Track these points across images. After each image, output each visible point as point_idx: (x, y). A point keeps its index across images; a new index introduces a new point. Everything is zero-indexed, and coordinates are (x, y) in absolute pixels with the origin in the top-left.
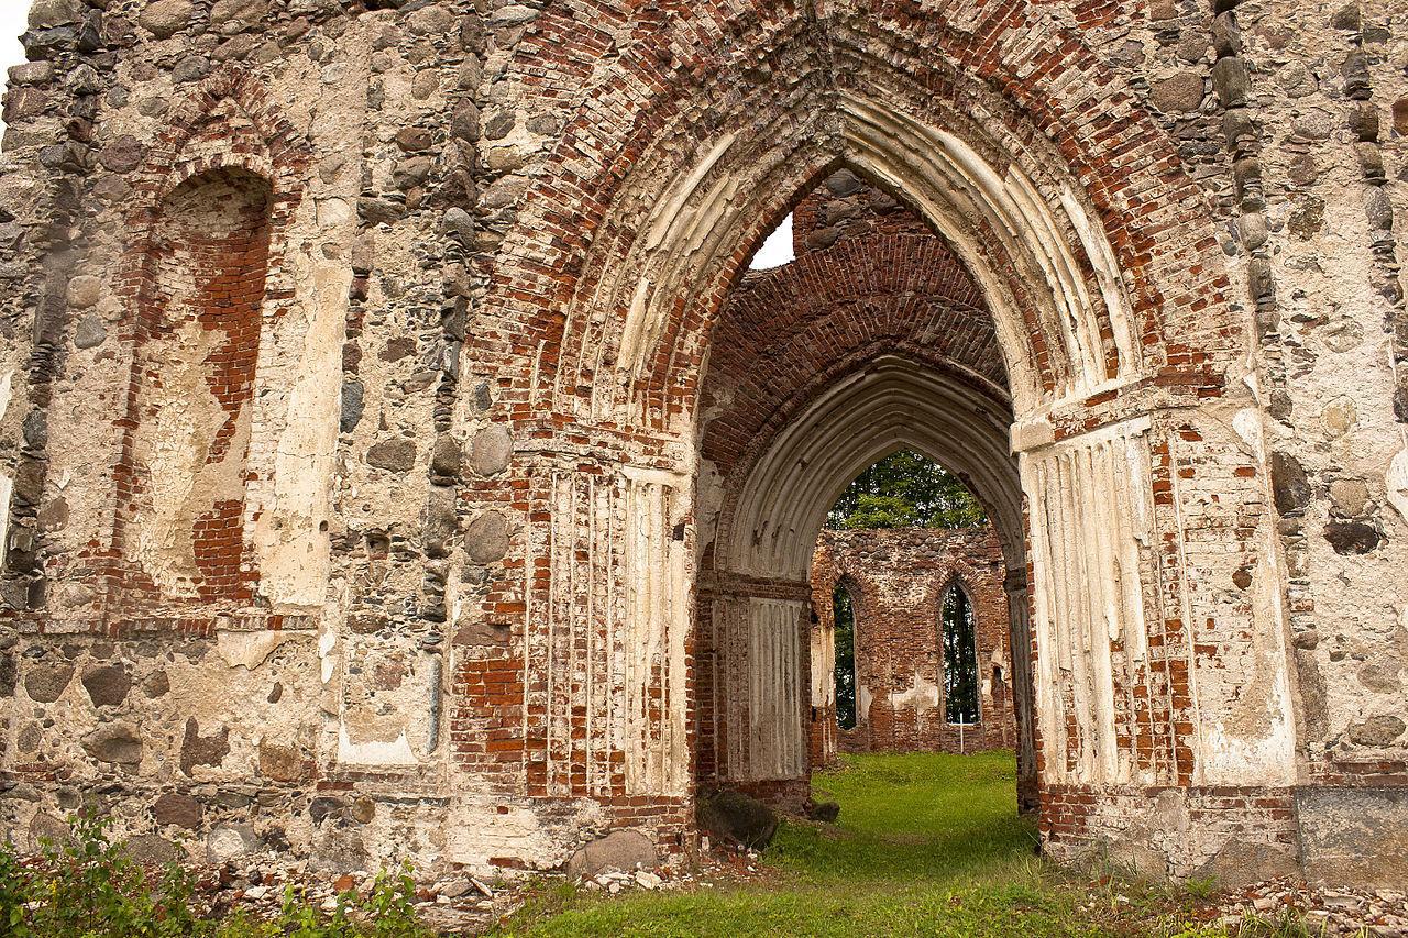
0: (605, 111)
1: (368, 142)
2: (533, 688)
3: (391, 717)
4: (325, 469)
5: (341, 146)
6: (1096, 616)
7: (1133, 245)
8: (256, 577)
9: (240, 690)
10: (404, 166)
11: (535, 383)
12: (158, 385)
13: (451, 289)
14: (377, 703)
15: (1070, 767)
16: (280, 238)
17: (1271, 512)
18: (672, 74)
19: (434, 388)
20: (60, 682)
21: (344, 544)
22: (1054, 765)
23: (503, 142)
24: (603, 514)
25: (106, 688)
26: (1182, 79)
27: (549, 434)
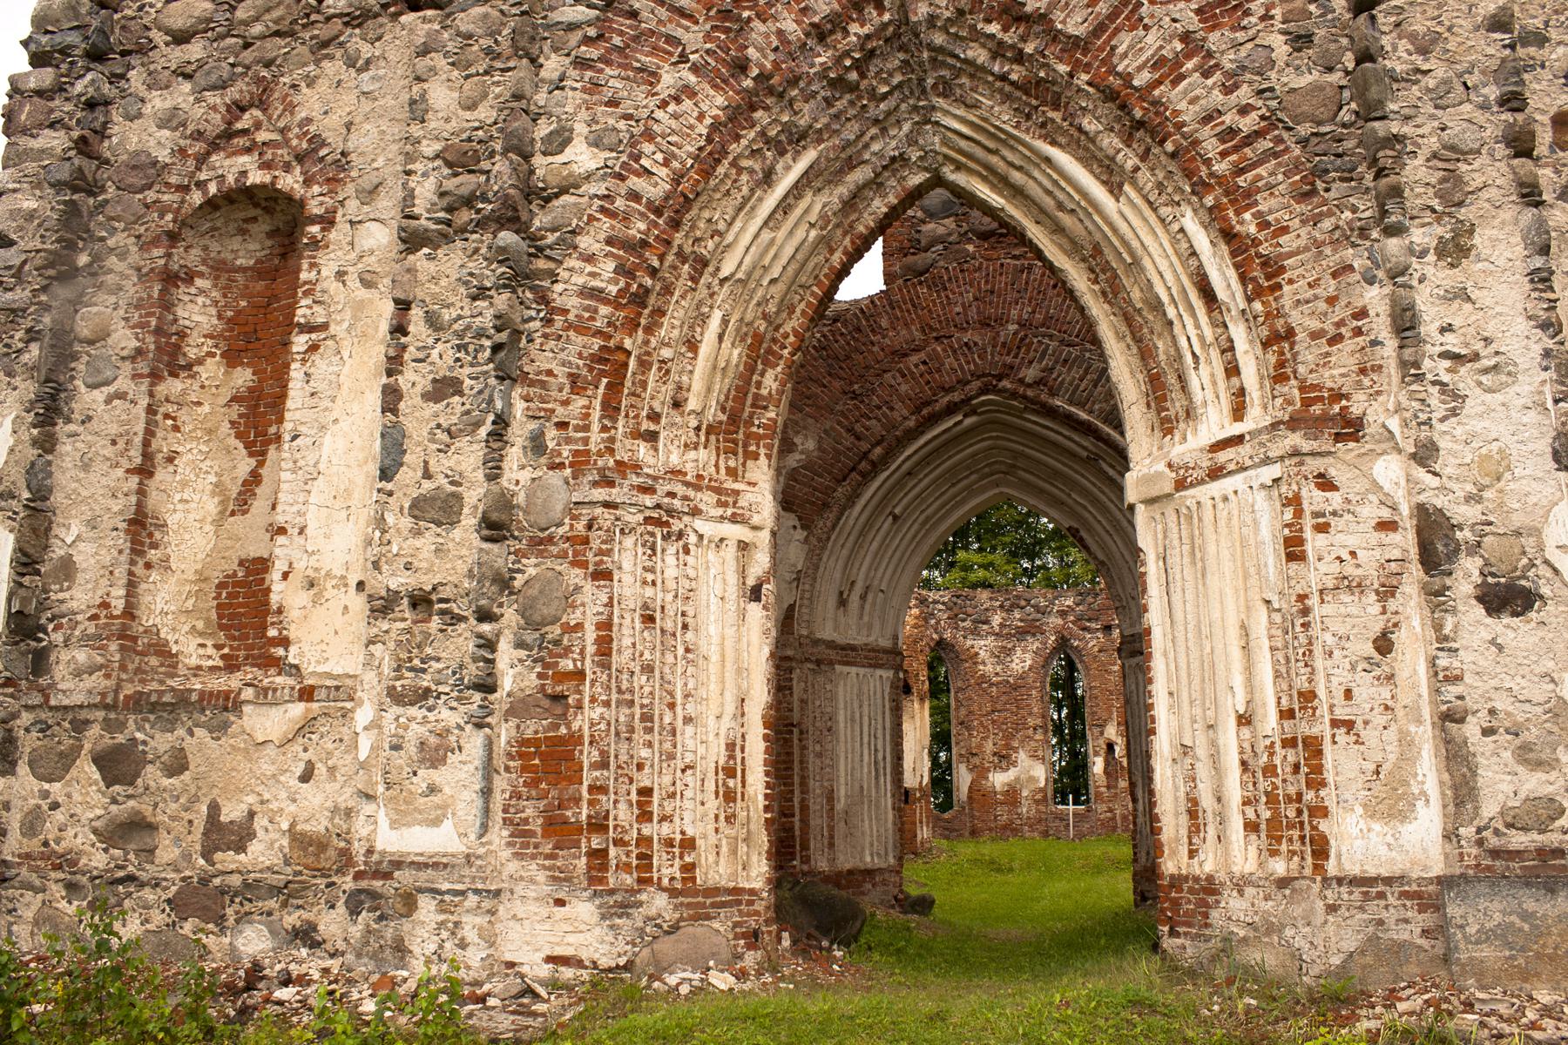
1: (409, 158)
2: (595, 766)
4: (362, 521)
5: (380, 162)
6: (1221, 686)
8: (285, 642)
9: (267, 768)
10: (450, 184)
11: (596, 427)
12: (176, 428)
13: (501, 322)
15: (1192, 854)
16: (312, 265)
17: (1415, 571)
19: (483, 432)
20: (67, 760)
21: (383, 606)
22: (1174, 853)
23: (560, 159)
24: (671, 572)
26: (1316, 88)
27: (611, 484)
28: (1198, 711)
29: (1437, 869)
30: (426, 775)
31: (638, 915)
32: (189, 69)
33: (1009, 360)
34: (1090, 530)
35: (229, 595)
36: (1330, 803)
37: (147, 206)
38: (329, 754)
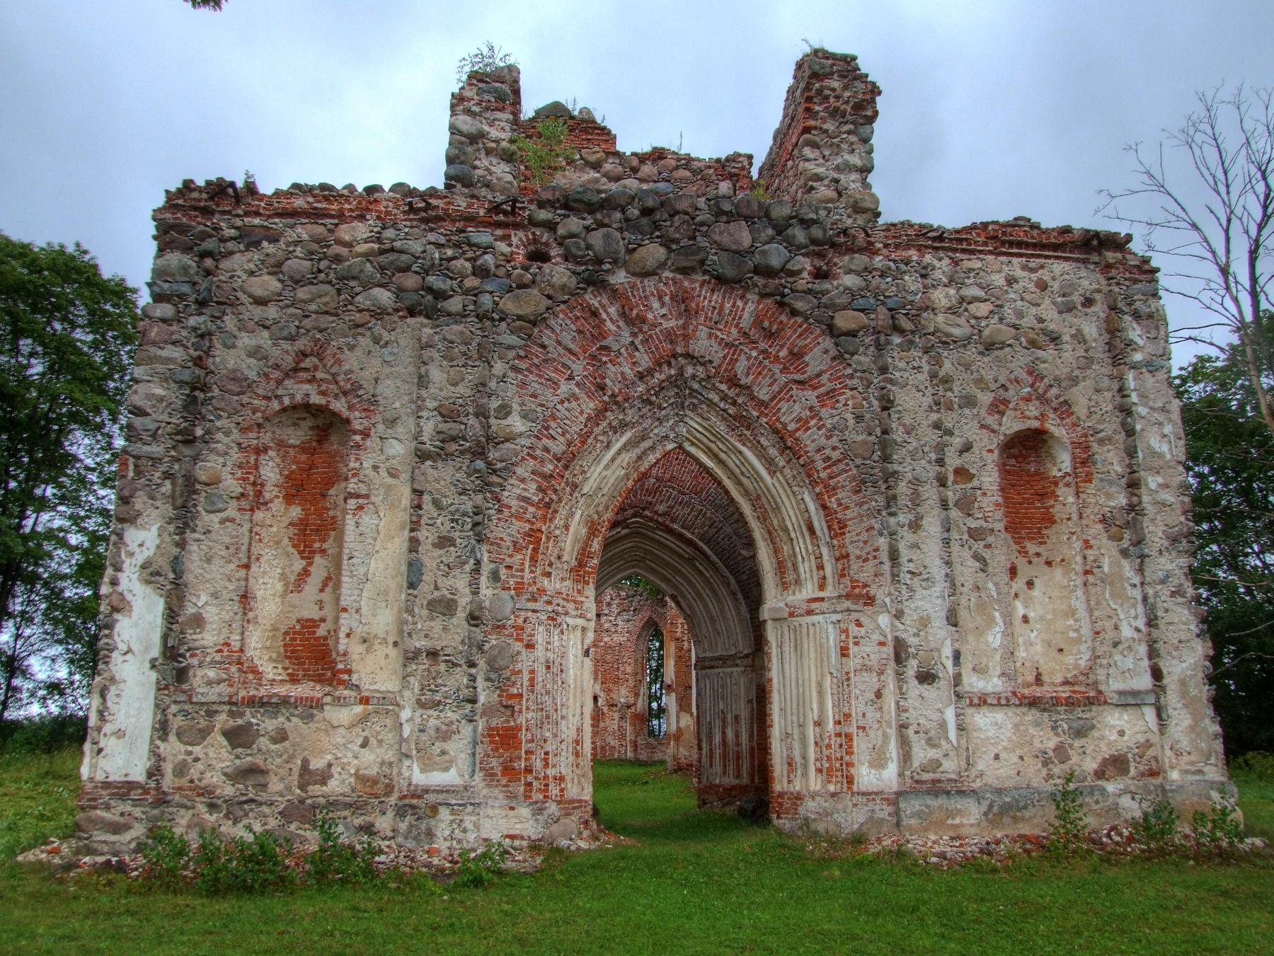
0: (567, 414)
1: (420, 408)
2: (527, 741)
3: (446, 758)
4: (395, 609)
5: (397, 405)
6: (808, 708)
7: (837, 527)
8: (349, 672)
9: (340, 740)
10: (444, 427)
11: (527, 570)
12: (260, 541)
13: (478, 511)
14: (437, 749)
15: (789, 782)
16: (357, 459)
17: (892, 664)
18: (606, 398)
19: (467, 568)
20: (204, 733)
21: (411, 657)
22: (781, 781)
23: (504, 422)
24: (556, 644)
25: (238, 737)
26: (865, 442)
27: (536, 600)
28: (795, 718)
29: (895, 788)
30: (438, 746)
31: (546, 813)
32: (268, 323)
33: (650, 499)
34: (684, 597)
35: (292, 639)
36: (855, 762)
37: (242, 405)
38: (378, 733)
